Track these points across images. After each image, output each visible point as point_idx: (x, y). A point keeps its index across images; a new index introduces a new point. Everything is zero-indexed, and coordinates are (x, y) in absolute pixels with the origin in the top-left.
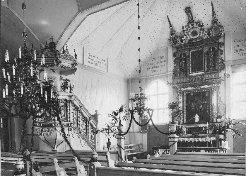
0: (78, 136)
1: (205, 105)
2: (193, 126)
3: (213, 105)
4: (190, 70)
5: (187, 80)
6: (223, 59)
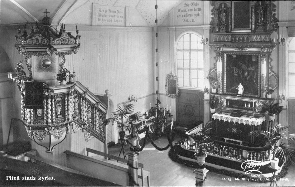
0: (81, 129)
1: (251, 73)
2: (236, 99)
3: (262, 75)
4: (233, 26)
5: (228, 39)
6: (276, 16)
